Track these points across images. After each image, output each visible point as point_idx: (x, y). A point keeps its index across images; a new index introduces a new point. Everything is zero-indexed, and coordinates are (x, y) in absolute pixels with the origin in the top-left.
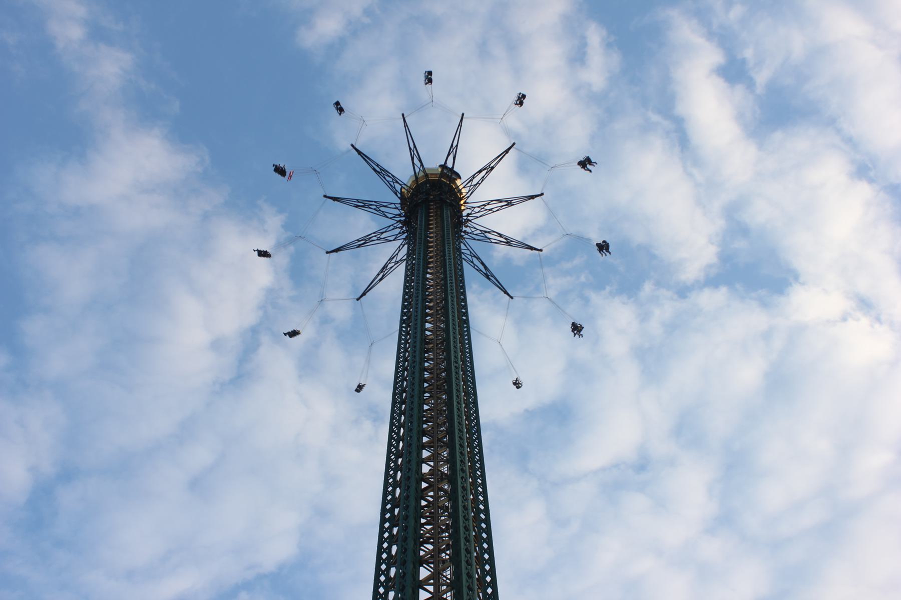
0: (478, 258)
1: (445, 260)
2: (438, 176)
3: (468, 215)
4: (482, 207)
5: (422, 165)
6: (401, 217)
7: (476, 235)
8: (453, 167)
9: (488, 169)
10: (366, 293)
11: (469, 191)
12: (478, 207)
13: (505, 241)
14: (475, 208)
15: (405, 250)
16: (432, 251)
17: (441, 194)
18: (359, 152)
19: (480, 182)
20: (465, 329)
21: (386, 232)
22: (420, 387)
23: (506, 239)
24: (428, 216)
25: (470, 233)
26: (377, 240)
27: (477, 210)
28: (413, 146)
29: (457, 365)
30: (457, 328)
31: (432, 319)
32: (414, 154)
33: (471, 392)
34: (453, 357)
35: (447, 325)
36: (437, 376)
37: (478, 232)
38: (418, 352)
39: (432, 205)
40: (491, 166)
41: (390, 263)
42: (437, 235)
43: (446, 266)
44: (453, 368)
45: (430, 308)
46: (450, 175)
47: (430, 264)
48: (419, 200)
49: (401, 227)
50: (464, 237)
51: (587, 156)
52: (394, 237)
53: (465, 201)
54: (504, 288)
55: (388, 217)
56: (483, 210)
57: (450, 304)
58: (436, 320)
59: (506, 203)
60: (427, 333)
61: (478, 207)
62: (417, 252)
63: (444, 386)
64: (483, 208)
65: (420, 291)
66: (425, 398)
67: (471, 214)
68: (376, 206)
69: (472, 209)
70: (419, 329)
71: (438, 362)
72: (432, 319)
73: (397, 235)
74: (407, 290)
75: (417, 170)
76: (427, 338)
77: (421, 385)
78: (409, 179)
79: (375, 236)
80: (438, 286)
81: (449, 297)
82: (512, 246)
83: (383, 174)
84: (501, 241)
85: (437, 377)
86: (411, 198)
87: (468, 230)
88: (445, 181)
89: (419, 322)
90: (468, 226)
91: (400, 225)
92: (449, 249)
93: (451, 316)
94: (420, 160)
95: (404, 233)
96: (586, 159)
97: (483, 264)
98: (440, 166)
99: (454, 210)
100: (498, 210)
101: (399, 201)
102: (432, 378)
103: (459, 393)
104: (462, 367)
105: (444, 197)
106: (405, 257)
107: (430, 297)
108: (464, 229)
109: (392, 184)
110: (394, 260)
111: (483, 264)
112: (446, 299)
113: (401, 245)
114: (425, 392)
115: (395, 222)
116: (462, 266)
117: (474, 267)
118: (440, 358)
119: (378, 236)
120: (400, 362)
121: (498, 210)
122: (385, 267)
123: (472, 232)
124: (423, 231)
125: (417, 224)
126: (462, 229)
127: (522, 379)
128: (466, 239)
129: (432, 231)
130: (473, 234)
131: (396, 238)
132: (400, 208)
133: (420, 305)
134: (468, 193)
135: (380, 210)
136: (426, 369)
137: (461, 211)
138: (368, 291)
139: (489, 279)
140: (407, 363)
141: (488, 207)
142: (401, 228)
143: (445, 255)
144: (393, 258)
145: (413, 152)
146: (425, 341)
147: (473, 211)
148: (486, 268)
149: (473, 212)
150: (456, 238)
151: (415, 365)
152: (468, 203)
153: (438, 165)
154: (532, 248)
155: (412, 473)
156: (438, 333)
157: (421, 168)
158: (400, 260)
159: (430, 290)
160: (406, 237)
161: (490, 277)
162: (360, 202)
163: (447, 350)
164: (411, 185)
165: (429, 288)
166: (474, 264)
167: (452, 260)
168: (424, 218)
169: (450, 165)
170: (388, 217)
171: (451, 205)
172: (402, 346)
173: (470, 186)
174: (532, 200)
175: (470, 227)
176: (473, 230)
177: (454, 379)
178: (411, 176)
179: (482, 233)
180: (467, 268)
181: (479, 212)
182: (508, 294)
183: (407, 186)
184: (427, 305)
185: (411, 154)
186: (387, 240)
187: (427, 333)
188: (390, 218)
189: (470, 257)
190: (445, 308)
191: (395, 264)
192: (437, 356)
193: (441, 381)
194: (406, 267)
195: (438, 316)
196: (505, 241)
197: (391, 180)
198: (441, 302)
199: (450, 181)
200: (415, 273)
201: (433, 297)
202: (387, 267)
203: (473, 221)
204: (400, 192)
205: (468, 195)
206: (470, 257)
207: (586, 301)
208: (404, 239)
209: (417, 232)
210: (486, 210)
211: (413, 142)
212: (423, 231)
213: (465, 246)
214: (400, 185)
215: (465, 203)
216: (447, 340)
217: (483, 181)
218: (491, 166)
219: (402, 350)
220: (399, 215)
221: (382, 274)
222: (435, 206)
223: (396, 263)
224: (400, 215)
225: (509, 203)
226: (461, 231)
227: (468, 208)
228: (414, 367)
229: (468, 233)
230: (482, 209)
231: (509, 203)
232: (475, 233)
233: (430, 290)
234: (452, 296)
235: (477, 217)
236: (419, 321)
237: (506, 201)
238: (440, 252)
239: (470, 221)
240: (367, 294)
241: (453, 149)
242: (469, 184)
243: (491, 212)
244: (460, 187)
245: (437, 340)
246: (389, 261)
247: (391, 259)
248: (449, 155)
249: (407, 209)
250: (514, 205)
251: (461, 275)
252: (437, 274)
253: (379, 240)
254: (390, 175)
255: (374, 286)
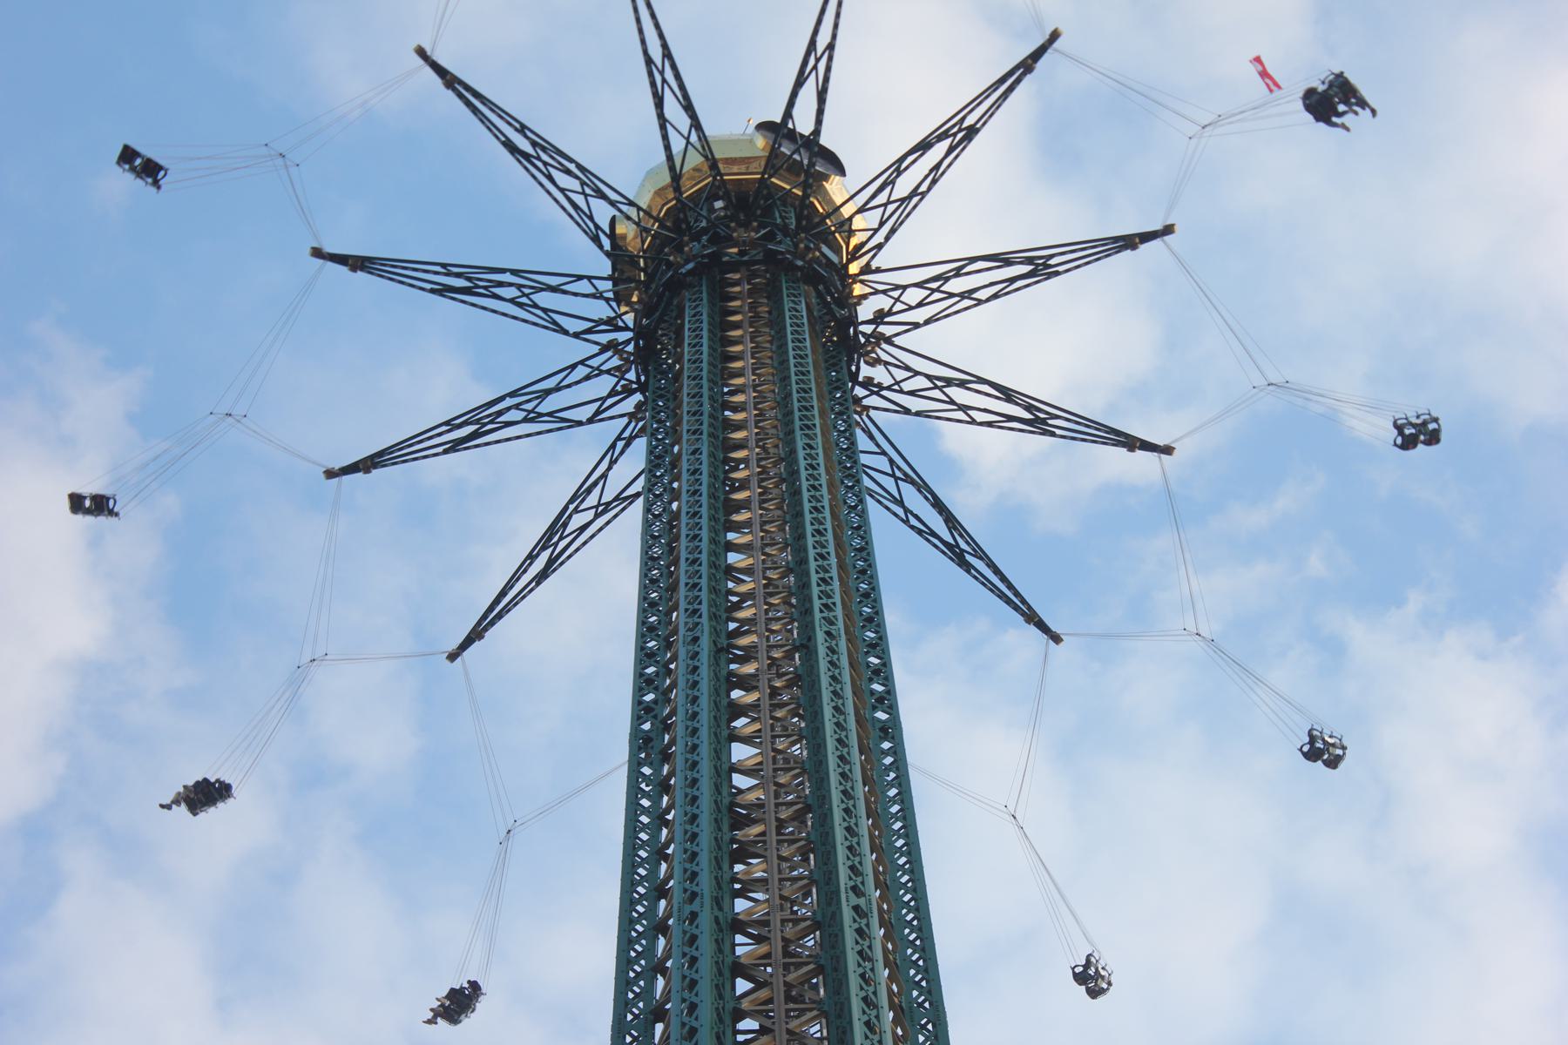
0: (922, 487)
1: (797, 493)
2: (755, 167)
3: (880, 317)
4: (934, 285)
5: (696, 124)
6: (618, 329)
7: (912, 393)
8: (817, 132)
9: (955, 135)
10: (486, 629)
11: (882, 224)
12: (919, 285)
13: (1027, 416)
14: (905, 288)
15: (635, 460)
16: (745, 460)
17: (770, 237)
18: (450, 80)
19: (923, 188)
20: (888, 760)
21: (558, 389)
22: (721, 997)
23: (1029, 408)
24: (721, 325)
25: (889, 388)
26: (525, 420)
27: (913, 296)
28: (660, 50)
29: (862, 902)
30: (856, 757)
31: (757, 726)
32: (664, 81)
33: (921, 1005)
34: (843, 873)
35: (817, 748)
36: (785, 948)
37: (921, 383)
38: (704, 859)
39: (736, 283)
40: (965, 125)
41: (576, 511)
42: (761, 398)
43: (800, 514)
44: (847, 914)
45: (746, 683)
46: (806, 162)
47: (737, 511)
48: (687, 262)
49: (618, 368)
50: (865, 402)
51: (1337, 71)
52: (589, 411)
53: (868, 264)
54: (1024, 601)
55: (566, 332)
56: (937, 296)
57: (823, 665)
58: (773, 729)
59: (1026, 269)
60: (740, 781)
61: (919, 285)
62: (685, 465)
63: (815, 987)
64: (937, 290)
65: (705, 620)
66: (740, 1038)
67: (890, 313)
68: (519, 287)
69: (896, 294)
70: (706, 768)
71: (786, 893)
72: (757, 726)
73: (604, 399)
74: (653, 643)
75: (677, 145)
76: (739, 799)
77: (722, 989)
78: (642, 185)
79: (517, 407)
80: (771, 595)
81: (820, 636)
82: (1053, 434)
83: (545, 164)
84: (1010, 418)
85: (786, 954)
86: (655, 253)
87: (880, 375)
88: (788, 187)
89: (706, 743)
90: (878, 361)
91: (616, 362)
92: (811, 453)
93: (828, 712)
94: (689, 108)
95: (628, 392)
96: (1331, 85)
97: (938, 505)
98: (764, 127)
99: (820, 295)
100: (996, 296)
101: (605, 267)
102: (768, 956)
103: (874, 1013)
104: (880, 910)
105: (782, 246)
106: (638, 486)
107: (744, 641)
108: (865, 371)
109: (579, 200)
110: (592, 500)
111: (938, 505)
112: (806, 646)
113: (619, 438)
114: (740, 1015)
115: (596, 349)
116: (863, 514)
117: (906, 522)
118: (795, 880)
119: (529, 406)
120: (639, 902)
121: (996, 296)
122: (557, 526)
123: (897, 383)
124: (705, 382)
125: (679, 360)
126: (858, 369)
127: (1109, 961)
128: (872, 413)
129: (738, 381)
130: (901, 391)
131: (598, 412)
132: (611, 295)
133: (704, 671)
134: (876, 231)
135: (536, 306)
136: (738, 925)
137: (849, 303)
138: (492, 623)
139: (967, 567)
140: (663, 903)
141: (955, 285)
142: (619, 372)
143: (794, 473)
144: (589, 491)
145: (662, 73)
146: (734, 814)
147: (897, 300)
148: (951, 520)
149: (899, 307)
150: (837, 408)
151: (695, 907)
152: (878, 270)
153: (753, 123)
154: (1131, 443)
155: (702, 903)
156: (782, 780)
157: (694, 138)
158: (616, 498)
159: (742, 615)
160: (639, 406)
161: (968, 557)
162: (458, 275)
163: (821, 845)
164: (649, 206)
165: (737, 606)
166: (907, 511)
167: (825, 490)
168: (705, 333)
169: (803, 123)
170: (566, 332)
171: (812, 278)
172: (643, 836)
173: (885, 205)
174: (1128, 253)
175: (886, 363)
176: (900, 374)
177: (852, 958)
178: (651, 173)
179: (936, 387)
180: (883, 526)
181: (920, 304)
182: (1042, 626)
183: (639, 209)
184: (731, 674)
185: (653, 84)
186: (563, 422)
187: (740, 781)
188: (576, 335)
189: (889, 483)
190: (805, 680)
191: (597, 516)
192: (780, 872)
193: (805, 969)
194: (647, 525)
195: (779, 714)
196: (1027, 416)
197: (575, 185)
198: (789, 656)
199: (805, 186)
200: (683, 548)
201: (753, 638)
202: (565, 525)
203: (897, 340)
204: (608, 231)
205: (879, 238)
206: (889, 483)
207: (1334, 650)
208: (631, 416)
209: (680, 389)
210: (951, 295)
211: (661, 36)
212: (705, 382)
213: (871, 437)
214: (613, 203)
215: (867, 269)
216: (817, 805)
217: (934, 182)
218: (965, 125)
219: (643, 854)
220: (609, 321)
221: (545, 556)
222: (747, 287)
223: (602, 509)
224: (613, 324)
225: (1040, 267)
226: (854, 377)
227: (877, 292)
228: (694, 916)
229: (879, 385)
230: (933, 291)
231: (1040, 267)
232: (906, 386)
233: (742, 615)
234: (828, 633)
235: (916, 326)
236: (704, 733)
237: (1029, 261)
238: (775, 464)
239: (889, 340)
240: (487, 634)
241: (818, 60)
242: (882, 198)
243: (967, 303)
244: (847, 211)
245: (777, 805)
246: (571, 501)
247: (579, 495)
248: (800, 82)
249: (639, 301)
250: (1057, 273)
251: (861, 550)
252: (768, 550)
253: (532, 420)
254: (572, 167)
255: (514, 603)
